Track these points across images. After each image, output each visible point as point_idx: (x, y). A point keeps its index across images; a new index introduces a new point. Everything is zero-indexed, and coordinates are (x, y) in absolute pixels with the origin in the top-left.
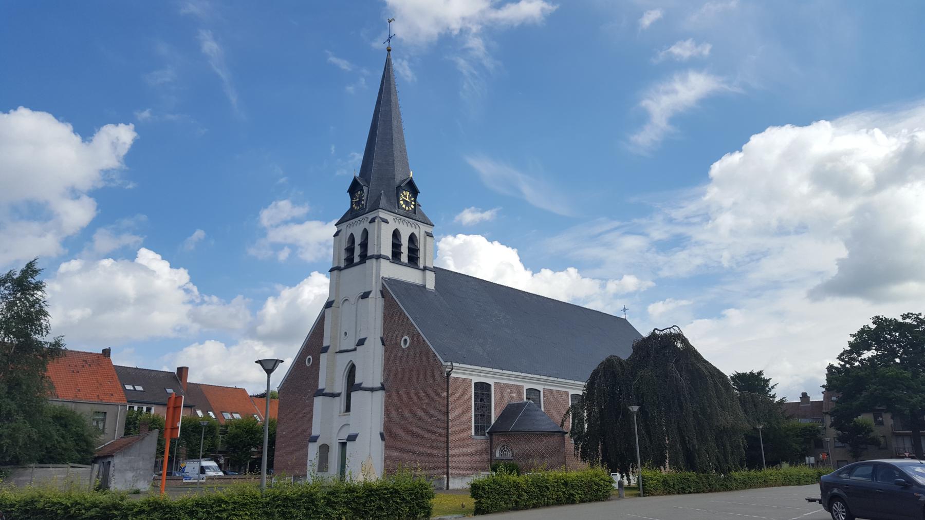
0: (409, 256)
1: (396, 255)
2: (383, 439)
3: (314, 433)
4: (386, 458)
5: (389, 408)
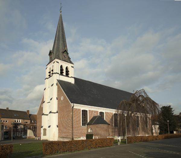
0: (66, 74)
1: (62, 73)
2: (57, 126)
3: (42, 126)
5: (59, 118)
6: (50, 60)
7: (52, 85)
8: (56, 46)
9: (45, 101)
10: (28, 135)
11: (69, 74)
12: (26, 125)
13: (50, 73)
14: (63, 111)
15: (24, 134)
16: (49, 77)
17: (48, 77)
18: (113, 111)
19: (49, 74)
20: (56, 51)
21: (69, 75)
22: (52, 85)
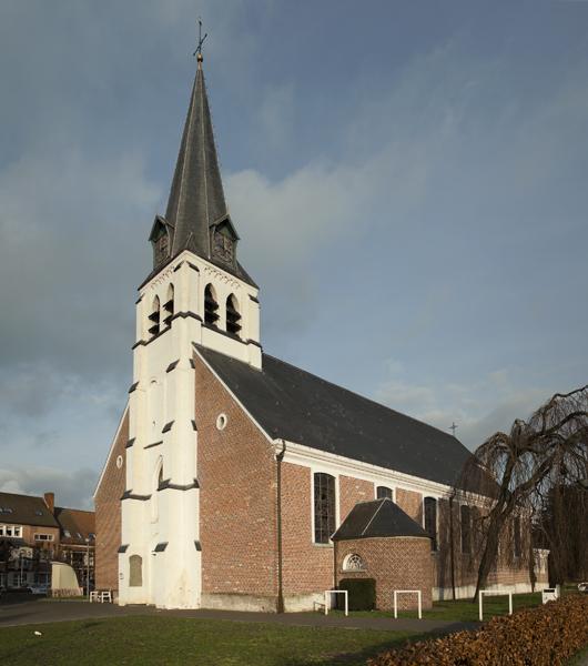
3: (124, 543)
4: (203, 573)
5: (205, 510)
6: (156, 261)
7: (171, 367)
8: (181, 200)
9: (133, 440)
10: (55, 585)
11: (239, 328)
12: (45, 546)
13: (158, 321)
14: (223, 476)
15: (36, 581)
16: (152, 335)
17: (148, 336)
18: (438, 491)
19: (152, 324)
20: (184, 220)
21: (241, 334)
22: (171, 367)
